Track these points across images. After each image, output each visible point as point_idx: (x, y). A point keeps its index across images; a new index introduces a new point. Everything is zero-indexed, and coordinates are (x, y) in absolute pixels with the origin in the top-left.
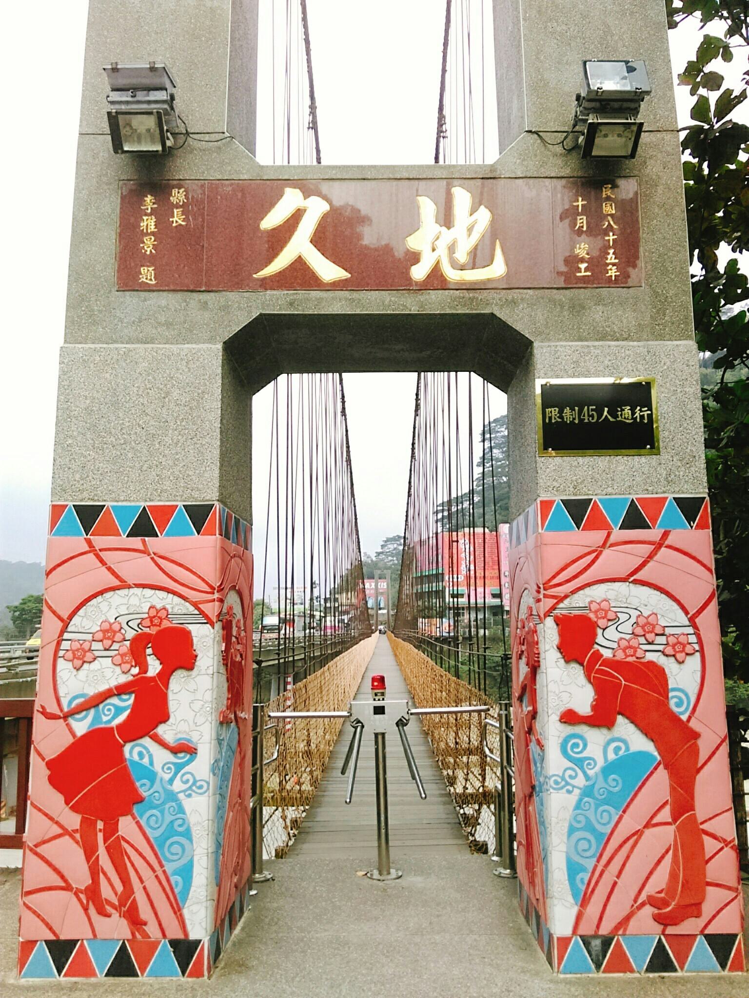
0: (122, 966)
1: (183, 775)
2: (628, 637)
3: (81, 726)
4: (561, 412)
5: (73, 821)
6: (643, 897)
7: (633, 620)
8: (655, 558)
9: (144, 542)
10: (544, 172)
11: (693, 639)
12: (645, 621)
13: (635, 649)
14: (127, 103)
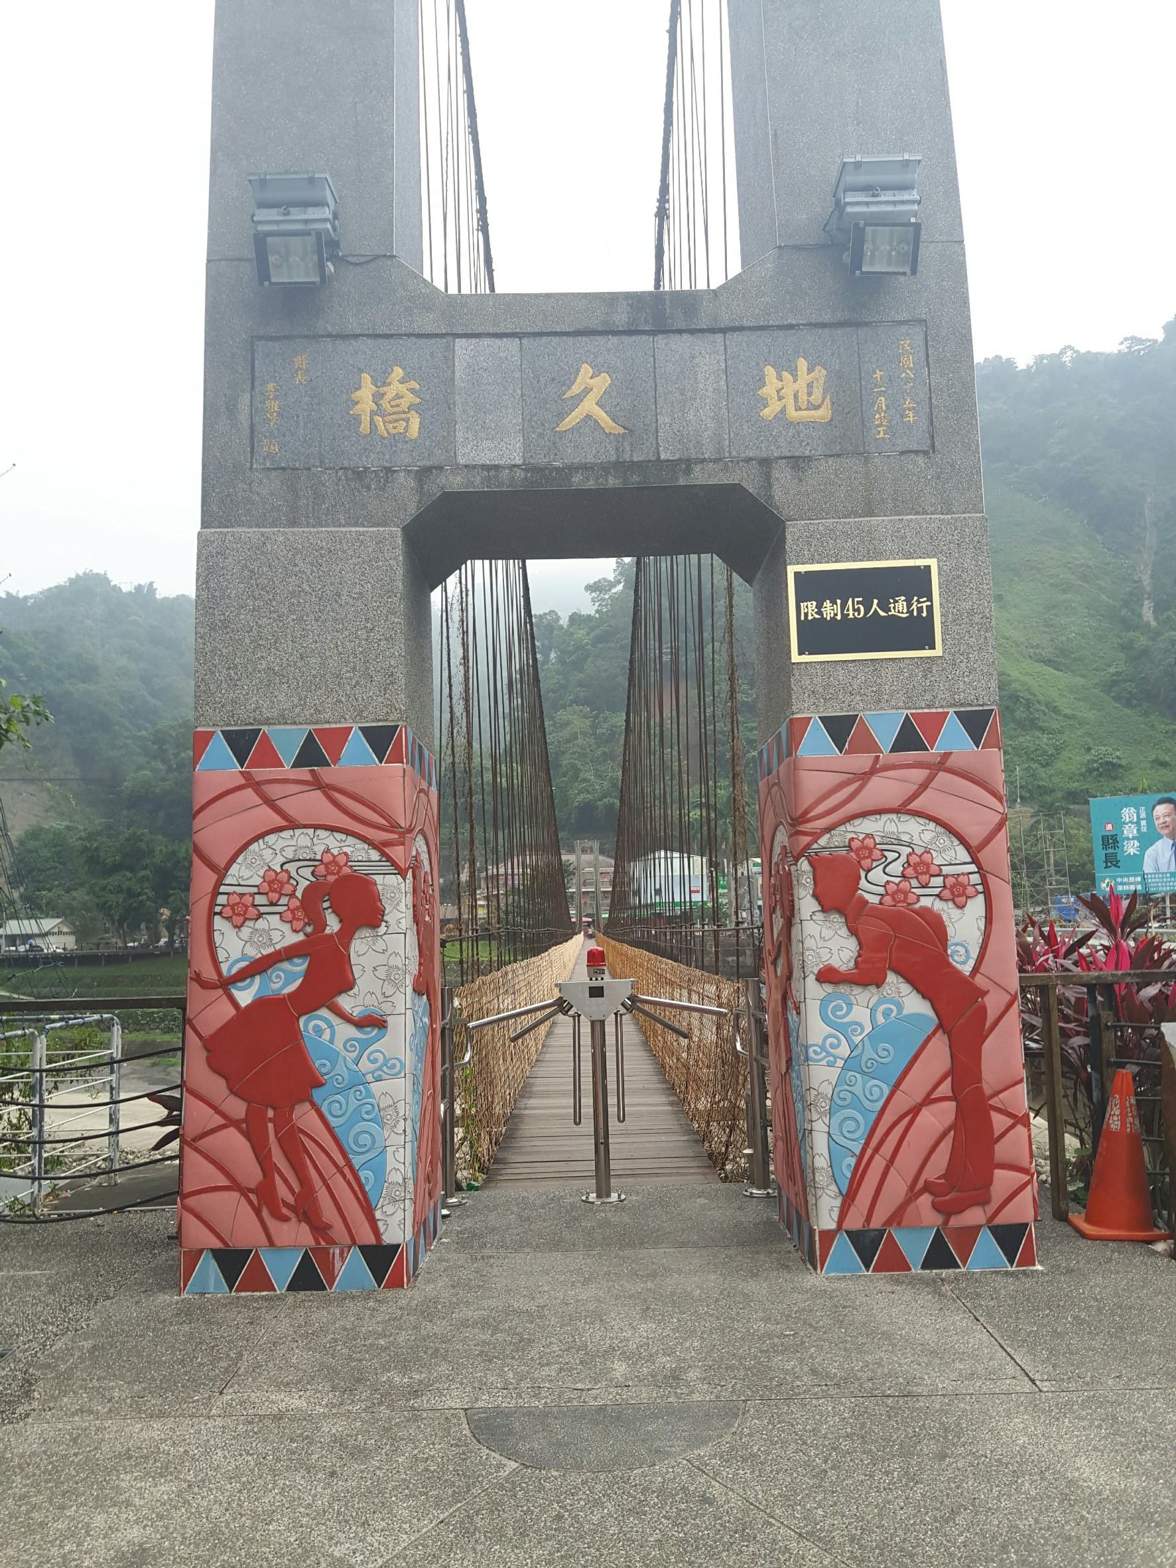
0: (309, 1278)
1: (372, 1053)
2: (897, 880)
3: (245, 996)
4: (819, 606)
5: (238, 1108)
6: (921, 1184)
7: (903, 859)
8: (932, 785)
9: (312, 772)
10: (827, 317)
11: (975, 879)
12: (918, 859)
13: (906, 893)
14: (278, 222)
